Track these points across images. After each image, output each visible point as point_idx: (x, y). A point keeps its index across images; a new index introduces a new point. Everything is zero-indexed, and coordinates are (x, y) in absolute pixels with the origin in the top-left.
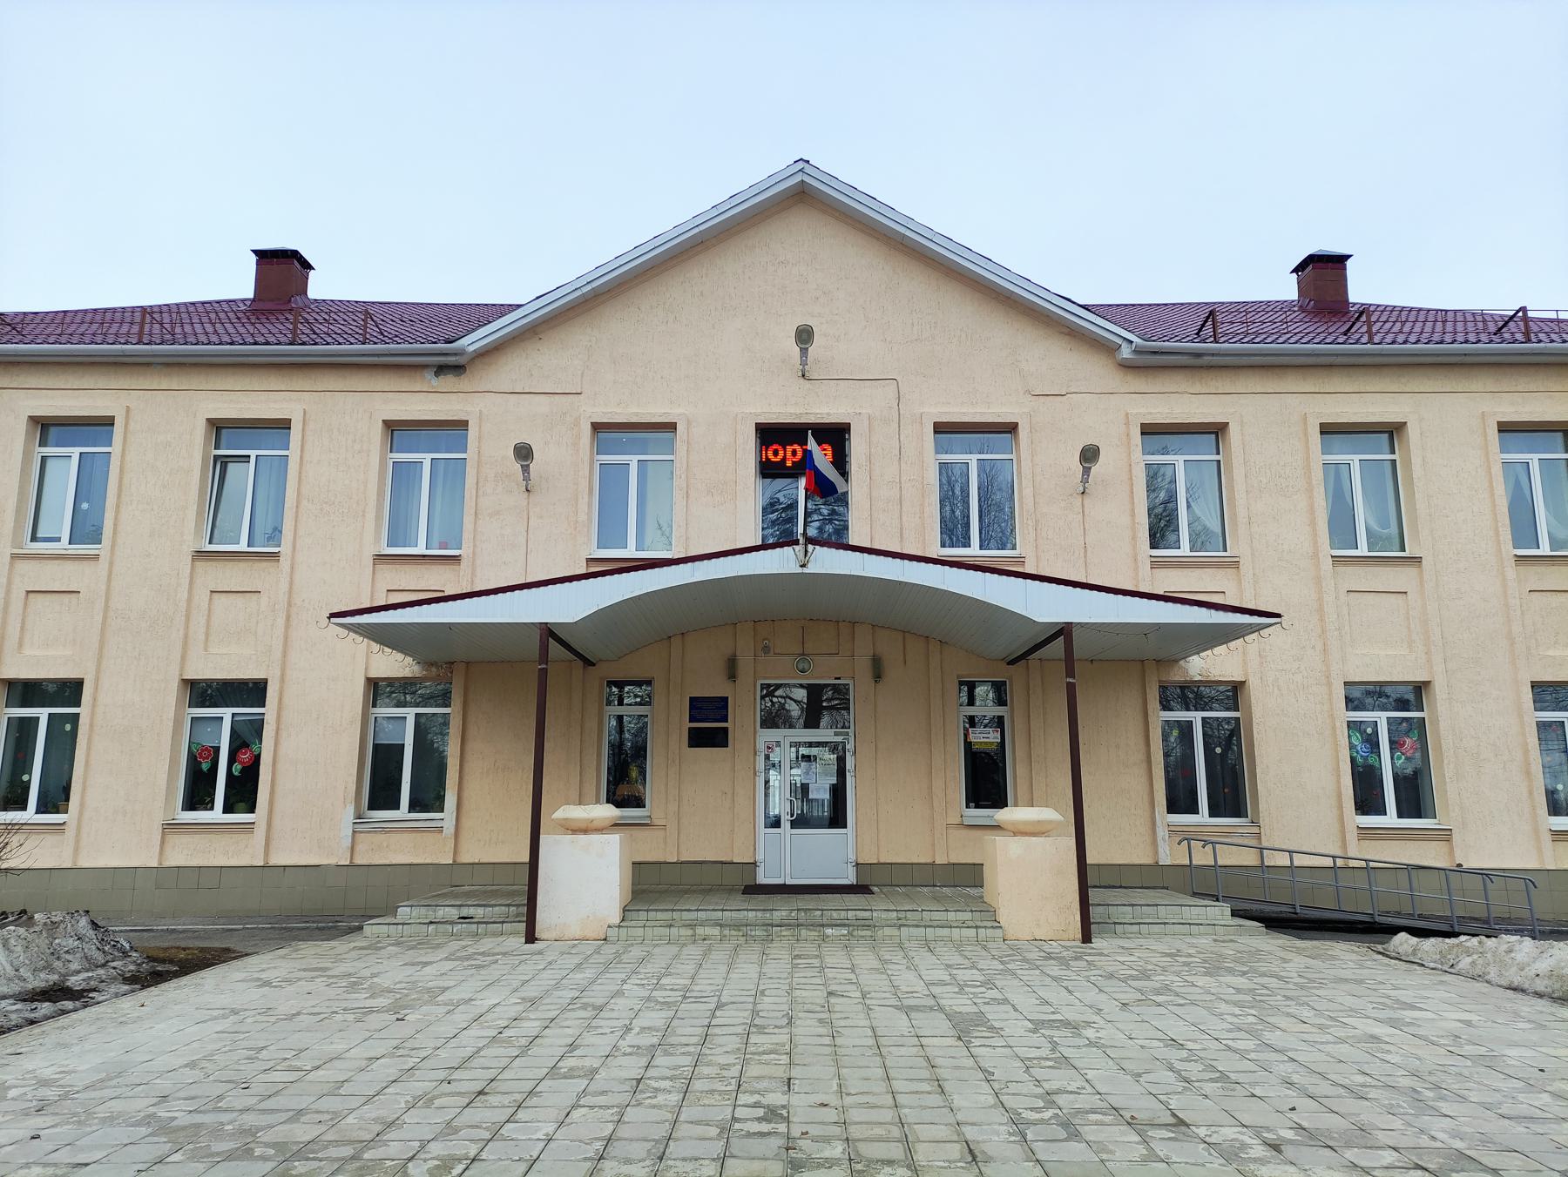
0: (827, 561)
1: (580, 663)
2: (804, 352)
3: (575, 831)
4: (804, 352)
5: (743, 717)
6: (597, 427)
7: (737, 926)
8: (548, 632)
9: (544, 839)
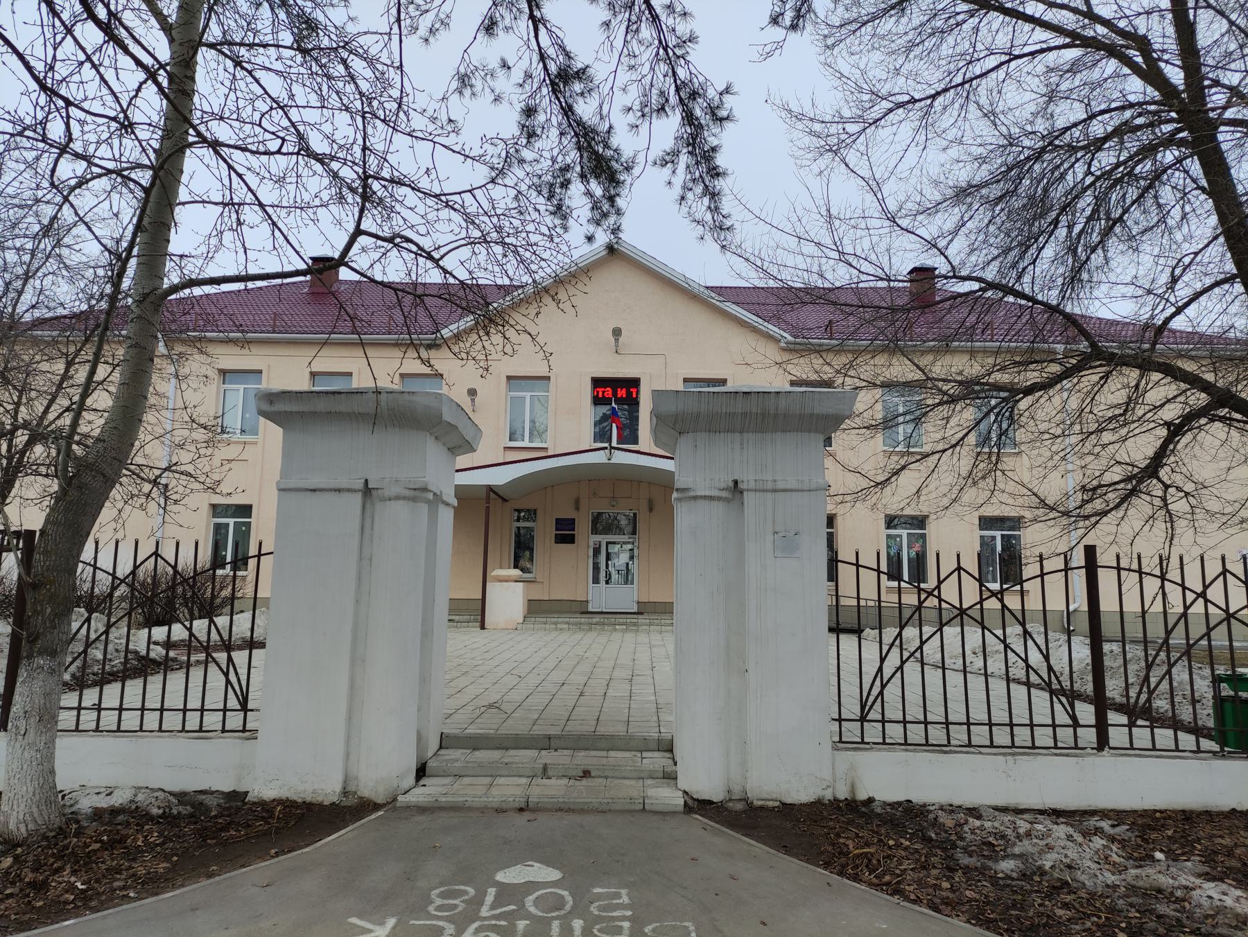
0: (621, 458)
1: (500, 500)
2: (617, 340)
3: (501, 581)
4: (617, 340)
5: (583, 528)
6: (509, 378)
7: (575, 624)
8: (490, 489)
9: (489, 585)
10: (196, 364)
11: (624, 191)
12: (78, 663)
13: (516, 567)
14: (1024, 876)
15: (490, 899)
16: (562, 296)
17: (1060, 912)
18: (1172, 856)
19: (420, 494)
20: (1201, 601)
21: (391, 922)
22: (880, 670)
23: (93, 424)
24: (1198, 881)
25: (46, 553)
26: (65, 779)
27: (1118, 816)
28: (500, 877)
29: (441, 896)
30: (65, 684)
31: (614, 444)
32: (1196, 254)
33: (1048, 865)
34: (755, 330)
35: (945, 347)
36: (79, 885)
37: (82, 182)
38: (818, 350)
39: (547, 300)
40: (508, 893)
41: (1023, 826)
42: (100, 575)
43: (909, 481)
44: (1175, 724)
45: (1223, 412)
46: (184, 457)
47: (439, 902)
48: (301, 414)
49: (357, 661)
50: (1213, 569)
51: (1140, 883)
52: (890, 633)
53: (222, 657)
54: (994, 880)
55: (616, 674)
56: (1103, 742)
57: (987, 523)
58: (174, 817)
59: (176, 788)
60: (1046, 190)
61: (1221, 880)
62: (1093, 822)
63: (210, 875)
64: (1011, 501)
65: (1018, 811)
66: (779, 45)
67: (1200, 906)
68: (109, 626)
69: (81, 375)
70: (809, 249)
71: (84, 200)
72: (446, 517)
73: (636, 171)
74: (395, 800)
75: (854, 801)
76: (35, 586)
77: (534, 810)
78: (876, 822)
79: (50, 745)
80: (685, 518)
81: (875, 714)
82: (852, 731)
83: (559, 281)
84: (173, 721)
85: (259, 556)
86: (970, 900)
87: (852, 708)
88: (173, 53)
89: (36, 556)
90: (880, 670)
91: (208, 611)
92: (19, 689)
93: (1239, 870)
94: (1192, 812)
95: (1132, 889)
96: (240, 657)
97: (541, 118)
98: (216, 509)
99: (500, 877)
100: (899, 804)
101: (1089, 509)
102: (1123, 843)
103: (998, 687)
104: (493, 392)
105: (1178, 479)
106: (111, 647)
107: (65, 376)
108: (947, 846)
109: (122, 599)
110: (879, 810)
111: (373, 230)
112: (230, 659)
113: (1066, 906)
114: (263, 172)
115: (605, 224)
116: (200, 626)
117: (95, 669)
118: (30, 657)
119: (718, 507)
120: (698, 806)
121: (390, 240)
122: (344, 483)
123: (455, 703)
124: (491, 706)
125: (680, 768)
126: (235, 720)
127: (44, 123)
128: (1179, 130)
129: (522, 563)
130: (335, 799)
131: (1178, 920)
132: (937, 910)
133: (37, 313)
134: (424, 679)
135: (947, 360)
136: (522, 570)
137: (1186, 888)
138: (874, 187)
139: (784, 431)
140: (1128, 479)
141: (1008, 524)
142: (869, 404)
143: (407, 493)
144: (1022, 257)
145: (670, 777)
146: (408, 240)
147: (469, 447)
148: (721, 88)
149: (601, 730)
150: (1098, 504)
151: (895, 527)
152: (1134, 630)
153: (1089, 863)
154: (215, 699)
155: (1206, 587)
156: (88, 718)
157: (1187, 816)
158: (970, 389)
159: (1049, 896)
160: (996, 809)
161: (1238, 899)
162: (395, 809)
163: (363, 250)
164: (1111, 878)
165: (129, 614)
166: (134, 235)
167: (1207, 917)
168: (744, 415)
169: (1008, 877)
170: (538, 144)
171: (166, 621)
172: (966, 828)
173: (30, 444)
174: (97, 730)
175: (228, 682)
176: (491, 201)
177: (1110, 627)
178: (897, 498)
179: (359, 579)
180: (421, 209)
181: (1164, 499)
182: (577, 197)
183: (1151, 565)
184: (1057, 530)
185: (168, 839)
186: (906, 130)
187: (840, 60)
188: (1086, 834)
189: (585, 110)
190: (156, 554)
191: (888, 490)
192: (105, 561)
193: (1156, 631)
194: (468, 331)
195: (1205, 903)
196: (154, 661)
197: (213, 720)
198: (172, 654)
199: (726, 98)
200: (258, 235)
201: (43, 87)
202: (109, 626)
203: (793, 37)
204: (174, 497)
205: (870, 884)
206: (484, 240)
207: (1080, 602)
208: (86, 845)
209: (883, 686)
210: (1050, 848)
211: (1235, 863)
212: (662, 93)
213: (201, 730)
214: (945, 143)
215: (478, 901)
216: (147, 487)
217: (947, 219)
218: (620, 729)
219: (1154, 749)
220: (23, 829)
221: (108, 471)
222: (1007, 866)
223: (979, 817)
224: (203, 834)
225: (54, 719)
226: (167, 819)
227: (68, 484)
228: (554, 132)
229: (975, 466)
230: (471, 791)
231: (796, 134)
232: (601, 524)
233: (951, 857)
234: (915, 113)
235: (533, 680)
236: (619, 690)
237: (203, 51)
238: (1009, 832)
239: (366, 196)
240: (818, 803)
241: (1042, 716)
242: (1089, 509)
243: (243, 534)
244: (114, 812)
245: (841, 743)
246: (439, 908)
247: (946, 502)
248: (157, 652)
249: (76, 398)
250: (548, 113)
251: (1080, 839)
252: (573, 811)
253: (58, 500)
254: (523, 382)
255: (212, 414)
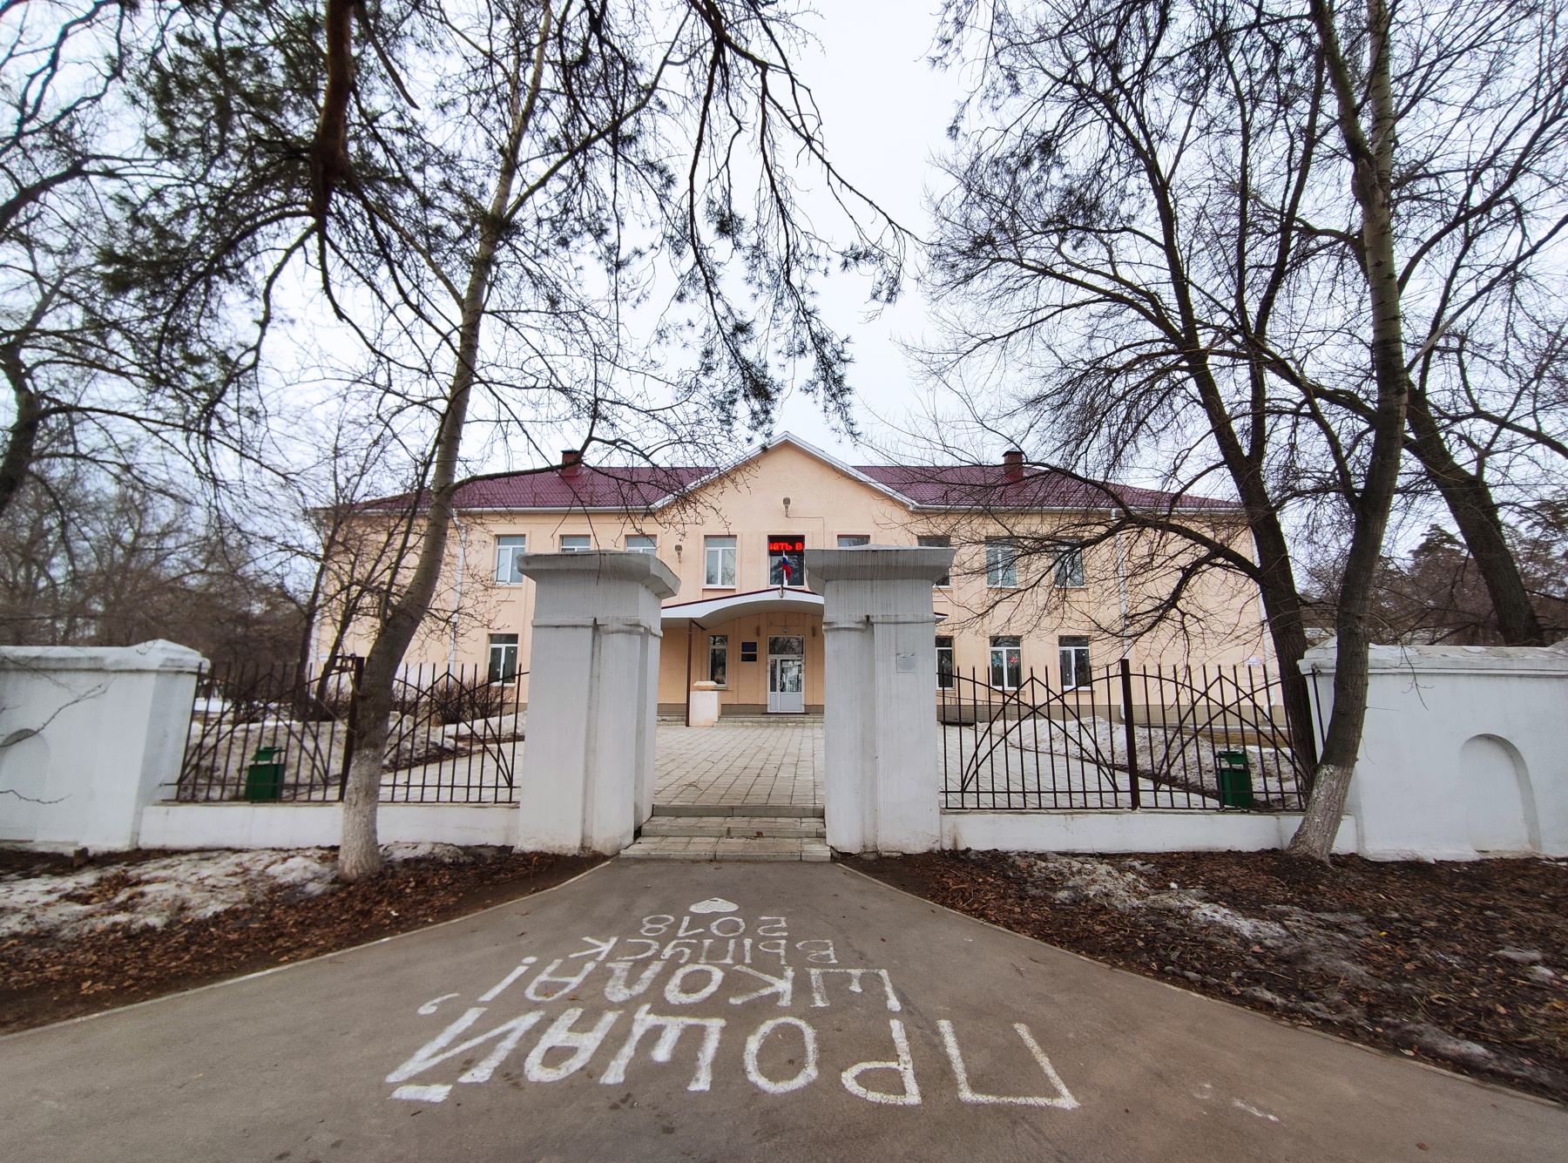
0: (791, 596)
5: (762, 650)
6: (706, 537)
8: (692, 621)
10: (477, 534)
11: (777, 405)
12: (394, 752)
13: (712, 679)
14: (1074, 902)
15: (685, 924)
16: (739, 478)
17: (1098, 928)
18: (1183, 886)
19: (633, 628)
20: (1204, 698)
21: (614, 940)
22: (976, 754)
23: (406, 577)
24: (1198, 903)
25: (371, 674)
26: (384, 836)
27: (1145, 857)
28: (693, 909)
29: (650, 922)
30: (385, 767)
31: (786, 585)
32: (1190, 449)
33: (1092, 894)
34: (891, 499)
35: (1022, 513)
36: (394, 913)
37: (400, 410)
38: (938, 513)
39: (727, 483)
40: (699, 920)
41: (1076, 865)
42: (408, 688)
43: (1003, 610)
44: (1187, 787)
45: (1220, 560)
46: (467, 602)
47: (648, 926)
48: (548, 571)
49: (590, 751)
50: (1212, 675)
51: (1157, 906)
52: (982, 727)
53: (494, 747)
54: (1053, 906)
55: (785, 760)
56: (1136, 803)
57: (1064, 641)
58: (461, 865)
59: (463, 844)
60: (1093, 399)
61: (1216, 902)
62: (1129, 862)
63: (486, 907)
64: (1075, 626)
65: (1074, 855)
66: (878, 313)
67: (1197, 921)
68: (416, 725)
69: (398, 542)
70: (924, 443)
71: (398, 423)
72: (654, 645)
73: (785, 392)
74: (618, 853)
75: (956, 851)
76: (363, 698)
77: (719, 861)
78: (971, 865)
79: (373, 811)
80: (831, 643)
81: (972, 787)
82: (955, 800)
83: (737, 469)
84: (460, 794)
85: (520, 674)
86: (1034, 920)
87: (955, 785)
88: (464, 319)
89: (365, 677)
90: (976, 754)
91: (485, 714)
92: (352, 772)
93: (1229, 895)
94: (1199, 853)
95: (1151, 910)
96: (507, 748)
97: (716, 357)
98: (493, 638)
99: (693, 909)
100: (989, 852)
101: (1130, 631)
102: (1148, 877)
103: (1060, 762)
104: (694, 546)
105: (1191, 609)
106: (417, 740)
107: (387, 544)
108: (1021, 882)
109: (426, 704)
110: (973, 857)
111: (601, 437)
112: (500, 750)
113: (1102, 923)
114: (525, 401)
115: (761, 429)
116: (479, 724)
117: (407, 756)
118: (359, 749)
119: (855, 636)
120: (841, 857)
121: (613, 443)
122: (578, 621)
123: (663, 783)
124: (690, 785)
125: (828, 831)
126: (504, 794)
127: (374, 373)
128: (1180, 360)
129: (717, 677)
130: (576, 852)
131: (1181, 931)
132: (1010, 928)
133: (368, 499)
134: (639, 766)
135: (1027, 521)
136: (718, 682)
137: (1189, 908)
138: (967, 399)
139: (903, 579)
140: (1156, 609)
141: (712, 571)
142: (969, 556)
143: (625, 628)
144: (1078, 446)
145: (821, 836)
146: (626, 443)
147: (671, 593)
148: (842, 339)
149: (772, 802)
150: (1137, 628)
151: (999, 645)
152: (1156, 718)
153: (1121, 892)
154: (489, 779)
155: (1207, 688)
156: (400, 793)
157: (1196, 856)
158: (1041, 545)
159: (1091, 917)
160: (1059, 854)
161: (1225, 916)
162: (619, 860)
163: (595, 450)
164: (1136, 902)
165: (429, 717)
166: (435, 447)
167: (1202, 928)
168: (873, 567)
169: (1063, 903)
170: (715, 375)
171: (456, 721)
172: (1035, 868)
173: (360, 595)
174: (406, 801)
175: (499, 766)
176: (686, 414)
177: (1139, 716)
178: (996, 623)
179: (591, 687)
180: (635, 421)
181: (1182, 623)
182: (743, 409)
183: (1167, 673)
184: (1106, 647)
185: (456, 880)
186: (990, 359)
187: (942, 310)
188: (1121, 871)
189: (749, 352)
190: (448, 674)
191: (986, 620)
192: (413, 680)
193: (1173, 719)
194: (669, 506)
195: (1201, 918)
196: (448, 750)
197: (488, 794)
198: (460, 745)
199: (846, 344)
200: (518, 441)
201: (374, 351)
202: (416, 725)
203: (888, 306)
204: (461, 631)
205: (963, 911)
206: (680, 441)
207: (1118, 700)
208: (399, 885)
209: (978, 766)
210: (1094, 881)
211: (1228, 890)
212: (802, 343)
213: (480, 802)
214: (1020, 366)
215: (677, 925)
216: (442, 624)
217: (1022, 421)
218: (785, 802)
219: (1173, 807)
220: (354, 871)
221: (414, 616)
222: (1063, 895)
223: (1045, 860)
224: (481, 877)
225: (376, 794)
226: (456, 866)
227: (386, 623)
228: (726, 367)
229: (1048, 600)
230: (674, 847)
231: (912, 362)
232: (776, 647)
233: (1023, 890)
234: (996, 347)
235: (723, 766)
236: (770, 770)
237: (484, 316)
238: (1066, 870)
239: (595, 415)
240: (930, 852)
241: (1092, 785)
242: (1130, 631)
243: (512, 655)
244: (418, 860)
245: (946, 810)
246: (648, 931)
247: (1029, 627)
248: (449, 744)
249: (394, 560)
250: (722, 354)
251: (1116, 874)
252: (749, 862)
253: (380, 635)
254: (717, 540)
255: (490, 568)
